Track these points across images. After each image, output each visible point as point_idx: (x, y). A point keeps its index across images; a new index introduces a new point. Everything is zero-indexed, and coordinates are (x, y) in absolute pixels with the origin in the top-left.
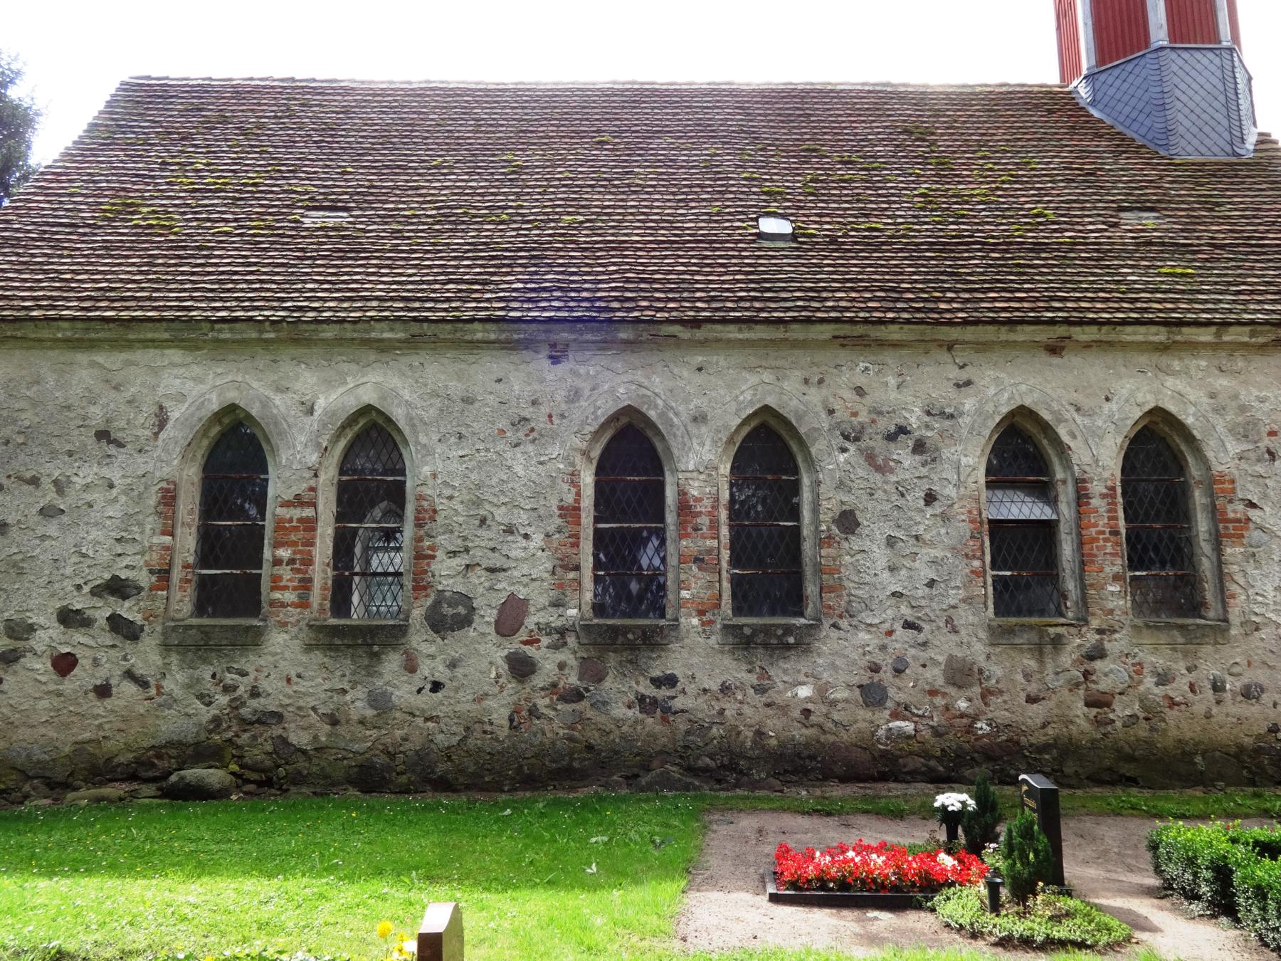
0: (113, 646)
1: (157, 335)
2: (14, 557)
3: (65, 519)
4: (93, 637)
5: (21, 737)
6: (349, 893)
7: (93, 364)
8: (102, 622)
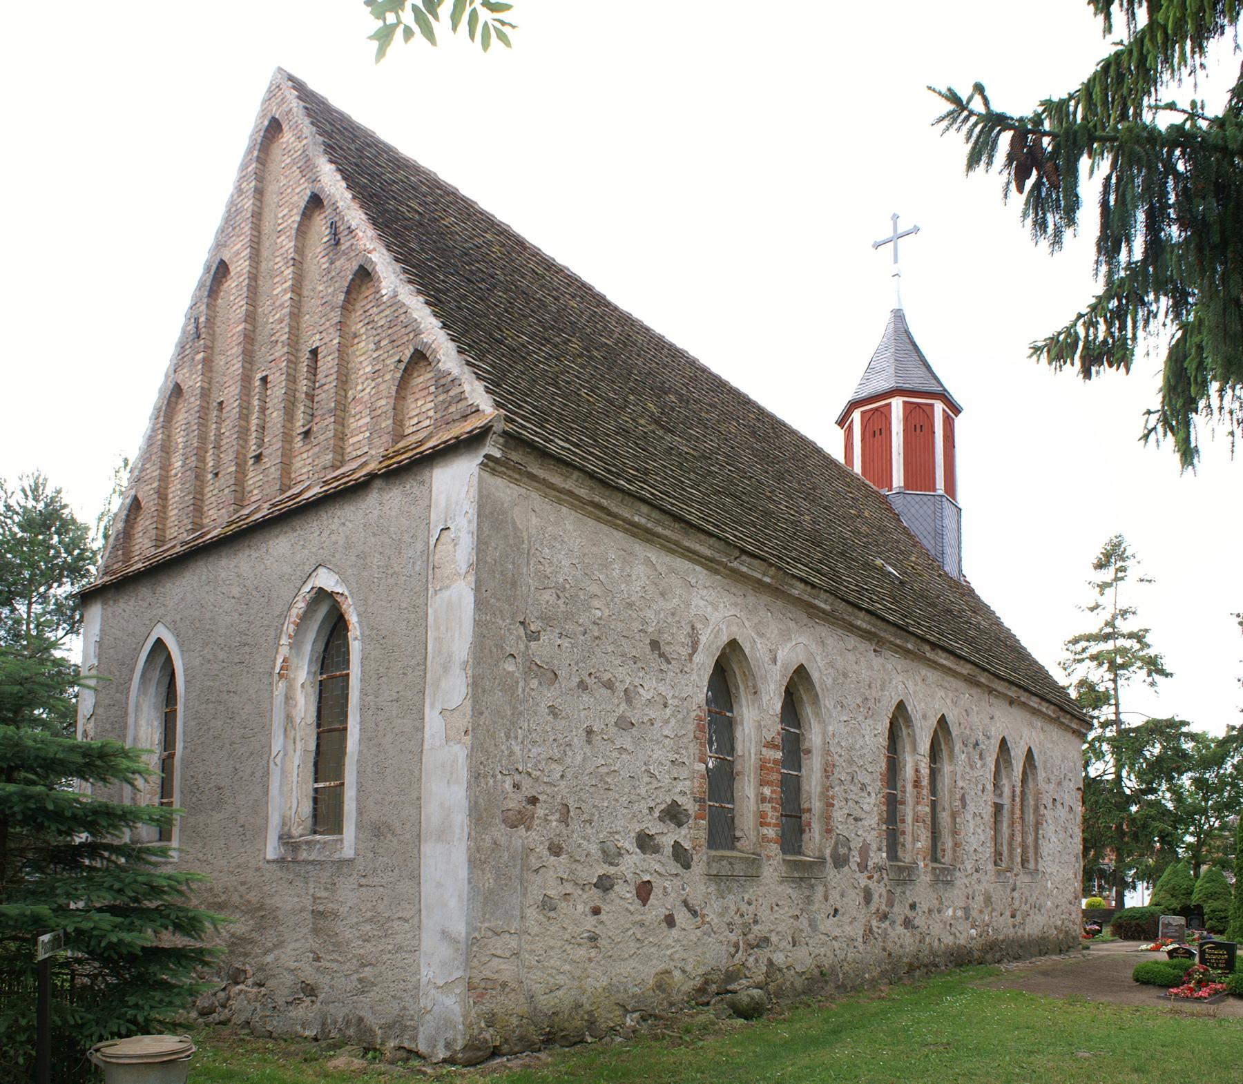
0: (677, 875)
1: (698, 547)
2: (601, 770)
3: (634, 731)
4: (664, 865)
5: (618, 972)
6: (224, 562)
7: (648, 561)
8: (668, 851)
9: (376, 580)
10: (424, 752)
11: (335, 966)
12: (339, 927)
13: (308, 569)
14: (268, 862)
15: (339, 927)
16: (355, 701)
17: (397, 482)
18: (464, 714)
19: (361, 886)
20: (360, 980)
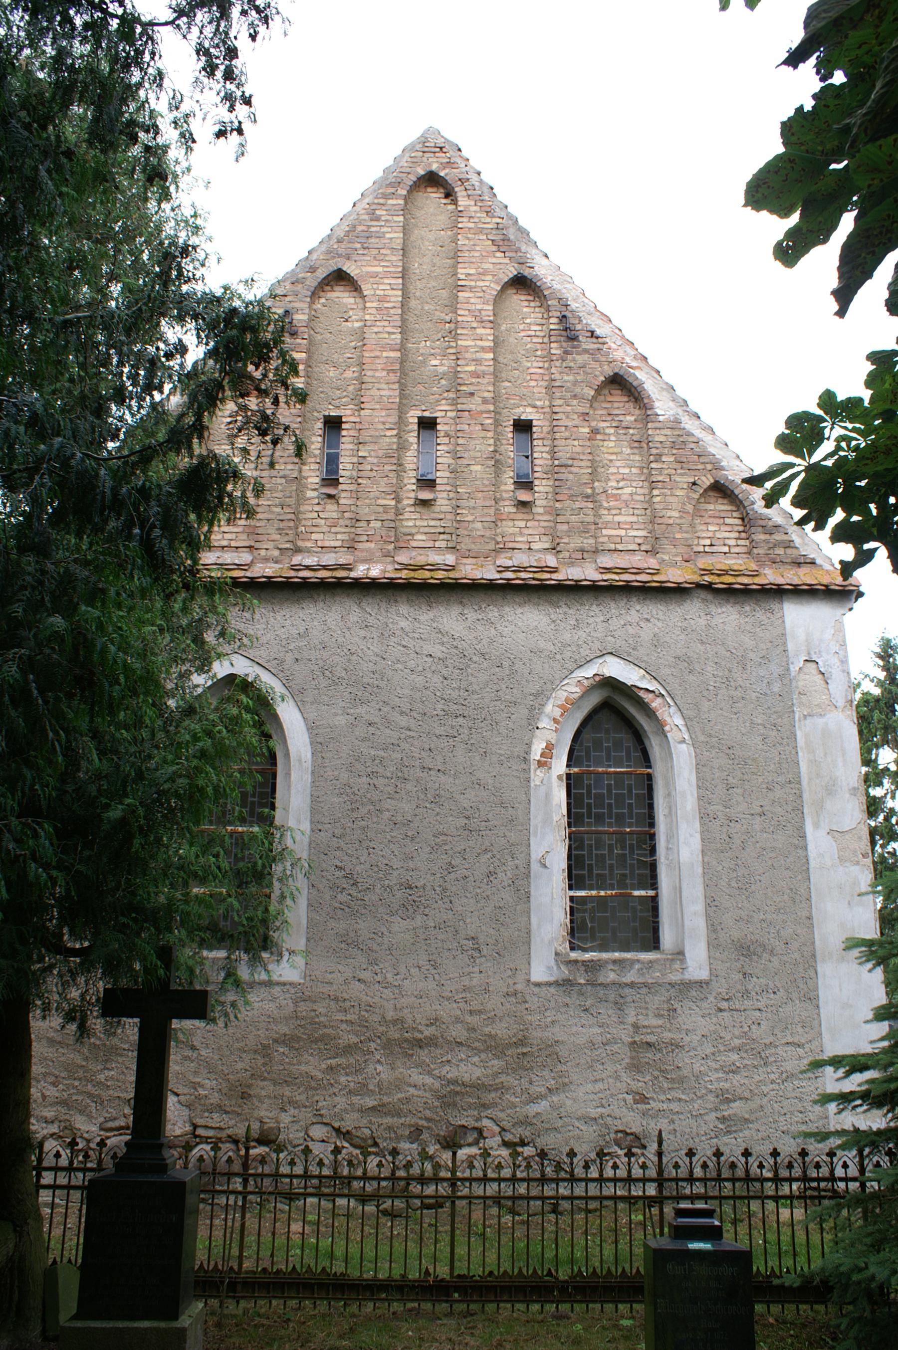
9: (711, 688)
10: (811, 870)
11: (675, 1106)
12: (683, 1059)
13: (643, 665)
14: (538, 985)
15: (683, 1059)
16: (689, 807)
17: (732, 600)
18: (860, 838)
19: (721, 1010)
20: (723, 1119)
